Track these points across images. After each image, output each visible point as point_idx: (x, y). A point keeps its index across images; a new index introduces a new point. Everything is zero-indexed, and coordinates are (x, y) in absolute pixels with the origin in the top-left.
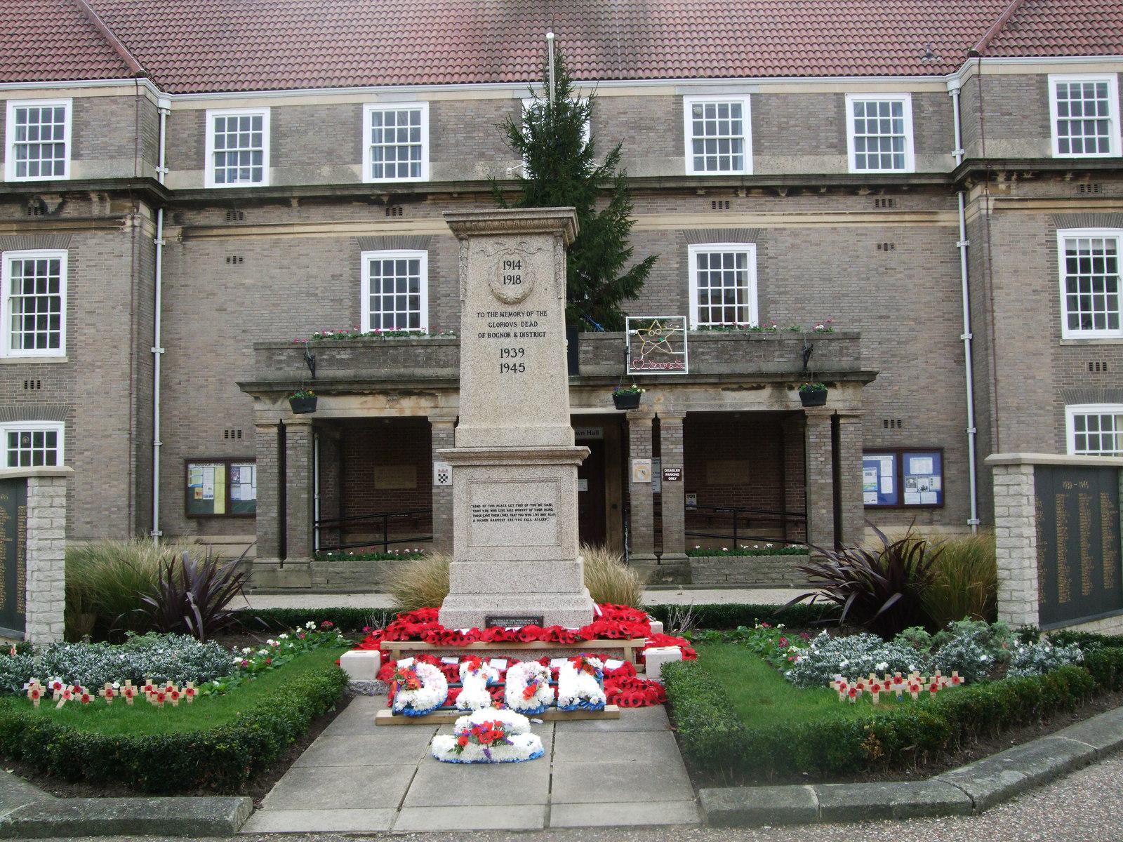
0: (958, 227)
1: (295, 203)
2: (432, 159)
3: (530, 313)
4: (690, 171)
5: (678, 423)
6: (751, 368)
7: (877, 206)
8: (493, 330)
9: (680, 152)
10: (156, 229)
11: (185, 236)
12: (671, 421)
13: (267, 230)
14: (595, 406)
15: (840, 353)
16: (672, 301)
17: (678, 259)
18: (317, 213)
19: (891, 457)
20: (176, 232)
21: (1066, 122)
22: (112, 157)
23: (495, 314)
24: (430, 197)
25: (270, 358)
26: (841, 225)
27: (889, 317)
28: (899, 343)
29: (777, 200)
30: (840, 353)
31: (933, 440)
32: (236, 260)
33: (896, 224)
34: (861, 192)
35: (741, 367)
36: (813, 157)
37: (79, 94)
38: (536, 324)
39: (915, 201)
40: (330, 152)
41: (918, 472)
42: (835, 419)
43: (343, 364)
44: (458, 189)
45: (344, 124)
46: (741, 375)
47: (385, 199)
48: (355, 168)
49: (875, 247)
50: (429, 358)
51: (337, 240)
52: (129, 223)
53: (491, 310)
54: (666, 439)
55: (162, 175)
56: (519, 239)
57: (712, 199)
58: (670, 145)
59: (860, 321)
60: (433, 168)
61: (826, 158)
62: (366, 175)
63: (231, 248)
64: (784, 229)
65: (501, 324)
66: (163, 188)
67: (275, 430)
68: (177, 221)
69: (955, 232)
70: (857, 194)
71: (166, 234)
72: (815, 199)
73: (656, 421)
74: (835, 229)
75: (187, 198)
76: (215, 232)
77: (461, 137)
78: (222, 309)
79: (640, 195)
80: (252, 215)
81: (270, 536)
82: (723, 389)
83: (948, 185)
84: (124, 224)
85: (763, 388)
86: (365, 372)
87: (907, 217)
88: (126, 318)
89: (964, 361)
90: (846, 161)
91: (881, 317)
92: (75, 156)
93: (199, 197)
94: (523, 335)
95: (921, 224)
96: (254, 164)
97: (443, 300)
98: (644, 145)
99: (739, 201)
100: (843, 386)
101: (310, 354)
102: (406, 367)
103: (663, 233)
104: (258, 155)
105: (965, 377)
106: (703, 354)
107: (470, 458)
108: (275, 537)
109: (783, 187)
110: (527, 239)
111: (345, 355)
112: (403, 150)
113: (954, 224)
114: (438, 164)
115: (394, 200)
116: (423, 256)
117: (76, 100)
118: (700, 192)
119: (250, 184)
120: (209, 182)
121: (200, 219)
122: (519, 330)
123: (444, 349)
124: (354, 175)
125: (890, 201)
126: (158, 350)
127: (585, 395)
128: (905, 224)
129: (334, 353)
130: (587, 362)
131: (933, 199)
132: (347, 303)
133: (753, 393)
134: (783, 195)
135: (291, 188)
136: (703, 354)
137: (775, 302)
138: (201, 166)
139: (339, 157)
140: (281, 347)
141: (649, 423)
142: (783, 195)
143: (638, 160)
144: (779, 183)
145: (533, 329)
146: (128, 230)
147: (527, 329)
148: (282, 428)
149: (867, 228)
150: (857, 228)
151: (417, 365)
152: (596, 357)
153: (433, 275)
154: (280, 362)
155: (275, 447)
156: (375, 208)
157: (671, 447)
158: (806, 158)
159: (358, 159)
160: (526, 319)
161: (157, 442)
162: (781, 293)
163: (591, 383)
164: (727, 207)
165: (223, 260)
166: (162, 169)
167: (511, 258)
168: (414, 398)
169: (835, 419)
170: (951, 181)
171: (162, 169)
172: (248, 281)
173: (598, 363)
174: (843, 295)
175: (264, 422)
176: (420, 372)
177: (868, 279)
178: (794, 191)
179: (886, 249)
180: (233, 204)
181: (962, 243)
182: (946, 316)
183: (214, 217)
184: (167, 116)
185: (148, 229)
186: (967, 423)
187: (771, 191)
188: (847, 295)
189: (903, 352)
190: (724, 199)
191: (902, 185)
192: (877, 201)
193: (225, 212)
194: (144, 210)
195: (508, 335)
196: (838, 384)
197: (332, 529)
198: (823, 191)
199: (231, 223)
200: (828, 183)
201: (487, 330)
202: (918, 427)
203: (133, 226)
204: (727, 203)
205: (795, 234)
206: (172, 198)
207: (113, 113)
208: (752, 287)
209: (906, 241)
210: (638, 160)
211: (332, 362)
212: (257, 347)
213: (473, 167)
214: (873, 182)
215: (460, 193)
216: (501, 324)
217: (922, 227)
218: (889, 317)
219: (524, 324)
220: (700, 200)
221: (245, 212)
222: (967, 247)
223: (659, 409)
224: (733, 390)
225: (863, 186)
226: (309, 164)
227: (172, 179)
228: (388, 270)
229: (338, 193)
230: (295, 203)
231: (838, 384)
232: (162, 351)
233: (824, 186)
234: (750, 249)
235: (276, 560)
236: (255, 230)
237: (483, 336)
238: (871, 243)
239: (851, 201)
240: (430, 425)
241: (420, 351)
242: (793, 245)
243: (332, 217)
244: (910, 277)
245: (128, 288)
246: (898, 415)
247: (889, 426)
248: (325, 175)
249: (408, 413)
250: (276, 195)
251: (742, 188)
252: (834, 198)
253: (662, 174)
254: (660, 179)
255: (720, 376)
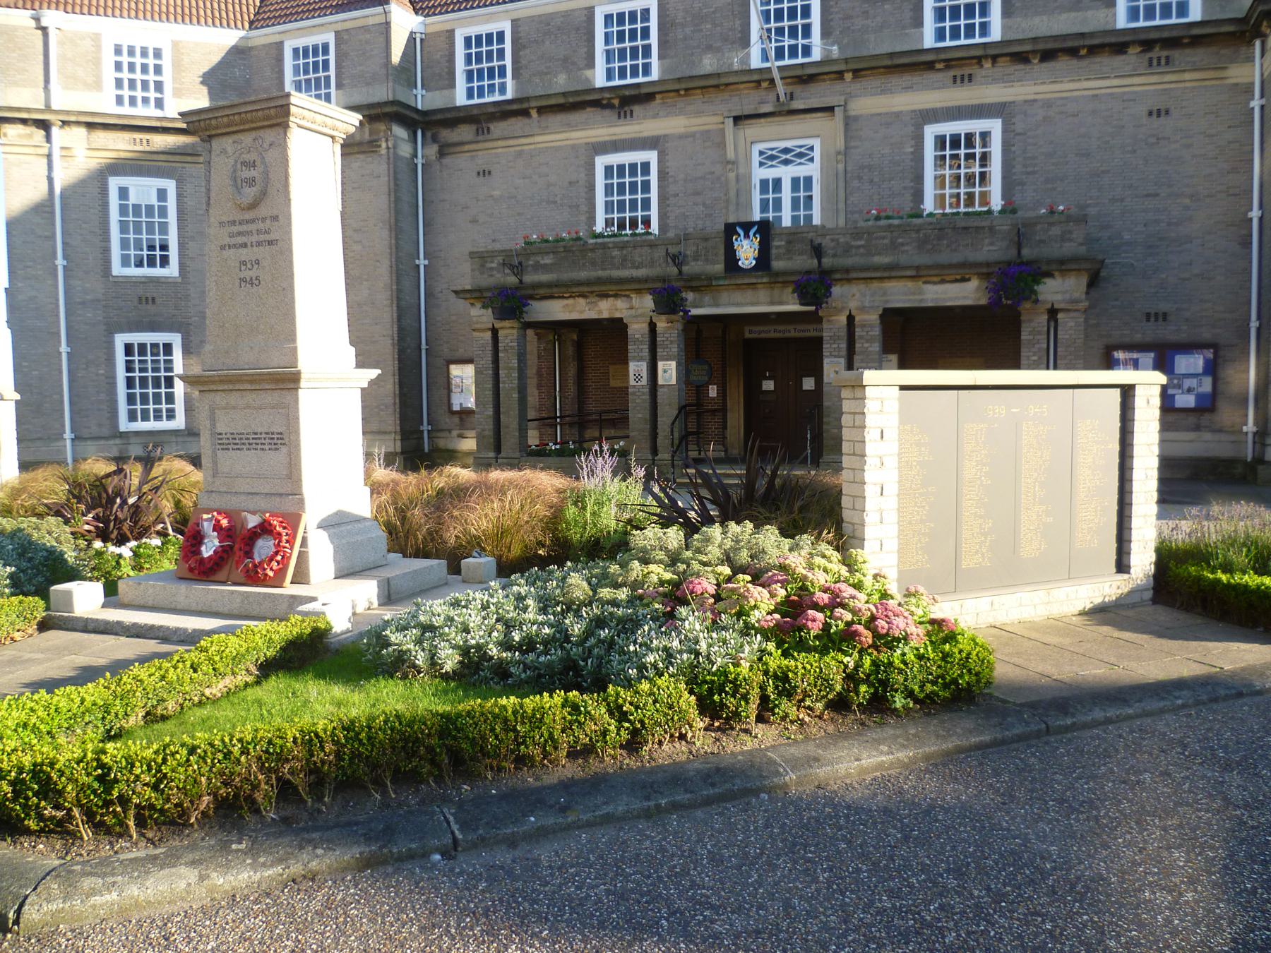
0: (1253, 84)
1: (534, 113)
2: (660, 57)
3: (264, 219)
4: (929, 41)
5: (874, 317)
6: (957, 258)
7: (1150, 65)
8: (233, 241)
9: (919, 23)
10: (416, 150)
11: (441, 154)
12: (866, 317)
13: (511, 142)
14: (787, 303)
15: (1064, 238)
16: (905, 188)
17: (913, 142)
18: (556, 120)
19: (1152, 355)
20: (433, 150)
21: (300, 81)
22: (368, 84)
23: (233, 223)
24: (658, 96)
25: (483, 266)
26: (1103, 91)
27: (1157, 195)
28: (1169, 224)
29: (1028, 67)
30: (1064, 238)
31: (1206, 335)
32: (485, 173)
33: (1173, 86)
34: (1131, 50)
35: (945, 257)
36: (1073, 14)
37: (339, 27)
38: (268, 232)
39: (1199, 55)
40: (565, 60)
41: (1183, 372)
42: (1053, 313)
43: (546, 268)
44: (684, 86)
45: (578, 29)
46: (942, 267)
47: (616, 102)
48: (588, 73)
49: (1145, 113)
50: (624, 259)
51: (573, 147)
52: (384, 145)
53: (231, 219)
54: (861, 337)
55: (419, 97)
56: (254, 134)
57: (952, 73)
58: (908, 15)
59: (1122, 200)
60: (661, 67)
61: (1090, 13)
62: (599, 79)
63: (480, 162)
64: (1035, 101)
65: (240, 234)
66: (417, 110)
67: (489, 334)
68: (435, 139)
69: (1249, 89)
70: (1125, 53)
71: (425, 152)
72: (1074, 62)
73: (851, 318)
74: (1096, 96)
75: (439, 117)
76: (466, 148)
77: (688, 30)
78: (474, 221)
79: (872, 75)
80: (498, 128)
81: (487, 433)
82: (925, 283)
83: (1243, 33)
84: (380, 146)
85: (969, 280)
86: (567, 275)
87: (1187, 76)
88: (385, 233)
89: (1251, 243)
90: (1115, 15)
91: (1148, 195)
92: (339, 86)
93: (448, 115)
94: (259, 244)
95: (1207, 83)
96: (951, 20)
97: (672, 201)
98: (879, 19)
99: (983, 72)
100: (1063, 276)
101: (515, 262)
102: (603, 269)
103: (898, 115)
104: (647, 49)
105: (1251, 262)
106: (902, 244)
107: (213, 382)
108: (491, 433)
109: (1034, 52)
110: (261, 133)
111: (547, 260)
112: (634, 50)
113: (1245, 80)
114: (667, 61)
115: (627, 101)
116: (652, 157)
117: (338, 34)
118: (938, 66)
119: (497, 97)
120: (461, 99)
121: (448, 135)
122: (254, 238)
123: (639, 250)
124: (587, 80)
125: (1167, 58)
126: (422, 262)
127: (776, 292)
128: (1184, 81)
129: (539, 258)
130: (778, 258)
131: (1223, 52)
132: (584, 208)
133: (957, 285)
134: (1036, 61)
135: (527, 99)
136: (902, 244)
137: (1022, 184)
138: (452, 85)
139: (574, 63)
140: (492, 254)
141: (843, 319)
142: (1036, 61)
143: (872, 37)
144: (1028, 48)
145: (267, 237)
146: (383, 151)
147: (262, 237)
148: (495, 331)
149: (1136, 92)
150: (1124, 93)
151: (613, 267)
152: (789, 251)
153: (662, 175)
154: (492, 269)
155: (490, 348)
156: (607, 112)
157: (866, 345)
158: (1065, 16)
159: (591, 64)
160: (261, 226)
161: (424, 346)
162: (1028, 173)
163: (780, 279)
164: (970, 81)
165: (475, 174)
166: (419, 91)
167: (246, 157)
168: (611, 300)
169: (1053, 313)
170: (1245, 28)
171: (419, 91)
172: (497, 193)
173: (790, 259)
174: (1103, 172)
175: (478, 326)
176: (616, 273)
177: (1135, 151)
178: (1048, 56)
179: (1159, 115)
180: (480, 119)
181: (1256, 104)
182: (1231, 191)
183: (464, 132)
184: (422, 40)
185: (405, 150)
186: (1250, 316)
187: (1021, 58)
188: (1108, 172)
189: (1173, 235)
190: (966, 71)
191: (1182, 37)
192: (1151, 60)
193: (474, 127)
194: (400, 132)
195: (245, 245)
196: (1056, 274)
197: (571, 425)
198: (1083, 52)
199: (480, 138)
200: (943, 56)
201: (227, 241)
202: (1187, 320)
203: (388, 148)
204: (970, 75)
205: (1048, 104)
206: (427, 119)
207: (367, 42)
208: (996, 169)
209: (1184, 103)
210: (872, 37)
211: (538, 267)
212: (472, 255)
213: (701, 60)
214: (1143, 37)
215: (686, 90)
216: (240, 234)
217: (1205, 87)
218: (1157, 195)
219: (259, 232)
220: (940, 75)
221: (492, 126)
222: (1262, 107)
223: (853, 305)
224: (935, 283)
225: (1134, 43)
226: (546, 74)
227: (422, 99)
228: (621, 173)
229: (571, 100)
230: (534, 113)
231: (1056, 274)
232: (427, 262)
233: (1084, 47)
234: (995, 126)
235: (492, 454)
236: (500, 143)
237: (223, 247)
238: (1142, 109)
239: (1118, 60)
240: (626, 326)
241: (616, 253)
242: (1045, 119)
243: (569, 125)
244: (1188, 146)
245: (386, 206)
246: (1163, 307)
247: (1152, 319)
248: (562, 82)
249: (605, 315)
250: (515, 107)
251: (986, 57)
252: (1098, 59)
253: (898, 49)
254: (892, 55)
255: (918, 268)
